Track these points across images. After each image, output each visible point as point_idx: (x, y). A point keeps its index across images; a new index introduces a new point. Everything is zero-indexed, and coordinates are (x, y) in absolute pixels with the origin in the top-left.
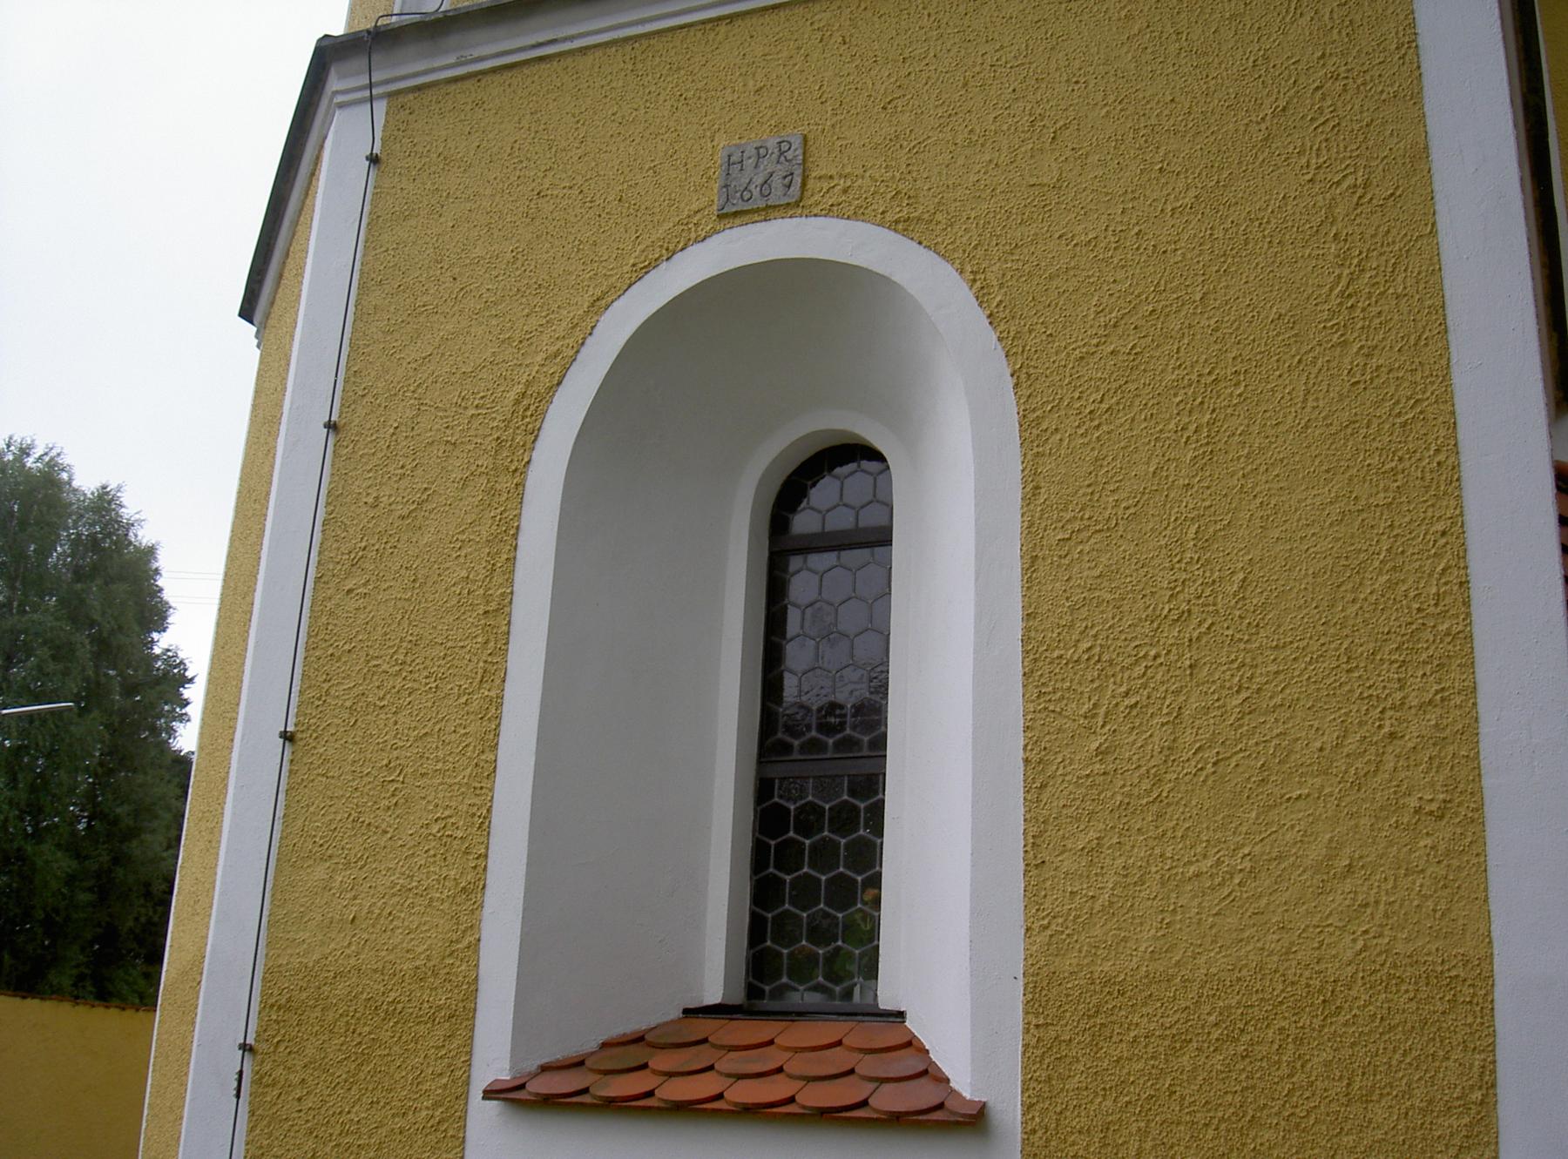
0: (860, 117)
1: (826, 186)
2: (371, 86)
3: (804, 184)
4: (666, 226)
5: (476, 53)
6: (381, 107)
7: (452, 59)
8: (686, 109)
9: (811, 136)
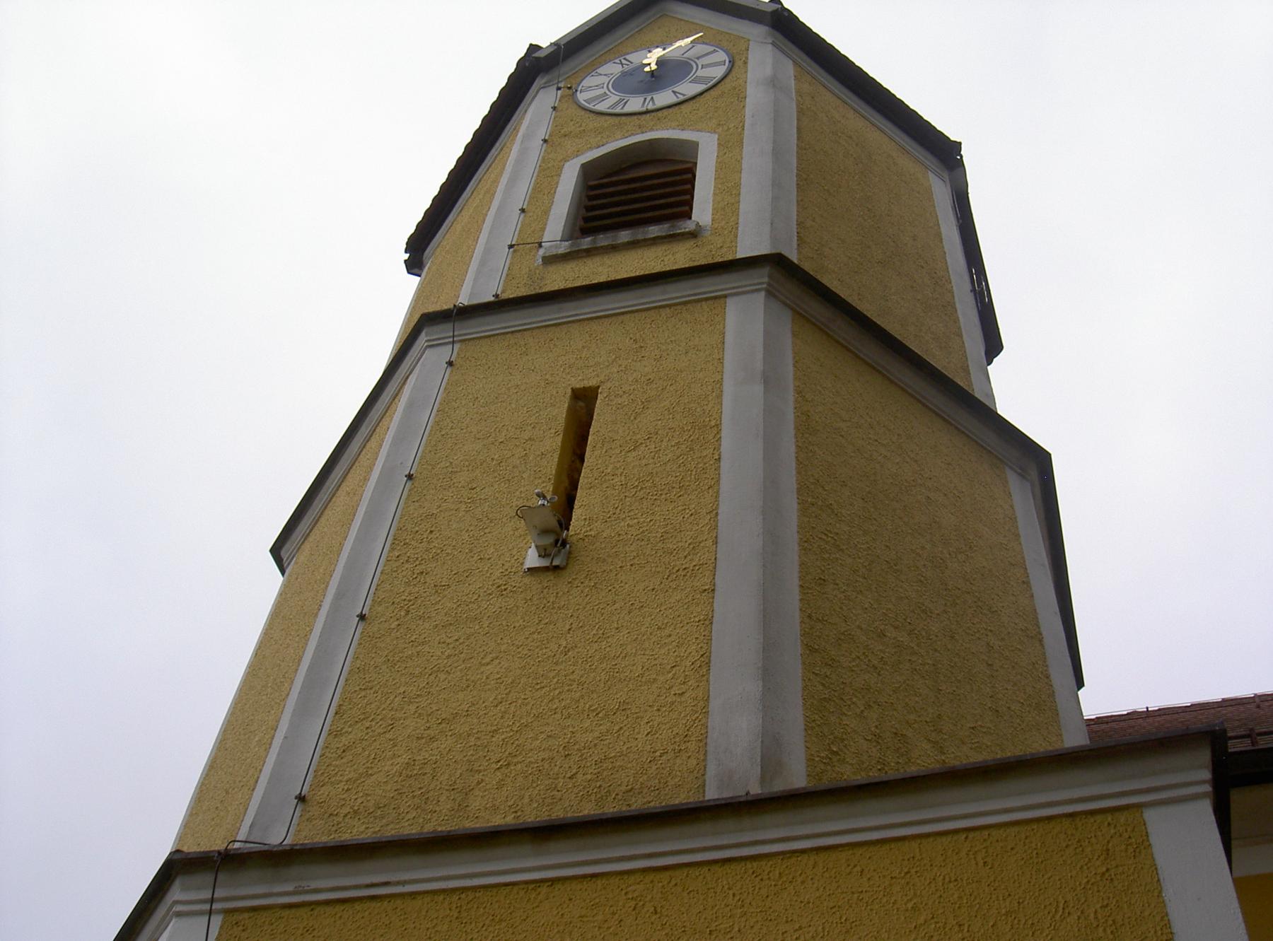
2: (212, 901)
5: (314, 884)
6: (217, 921)
7: (290, 888)
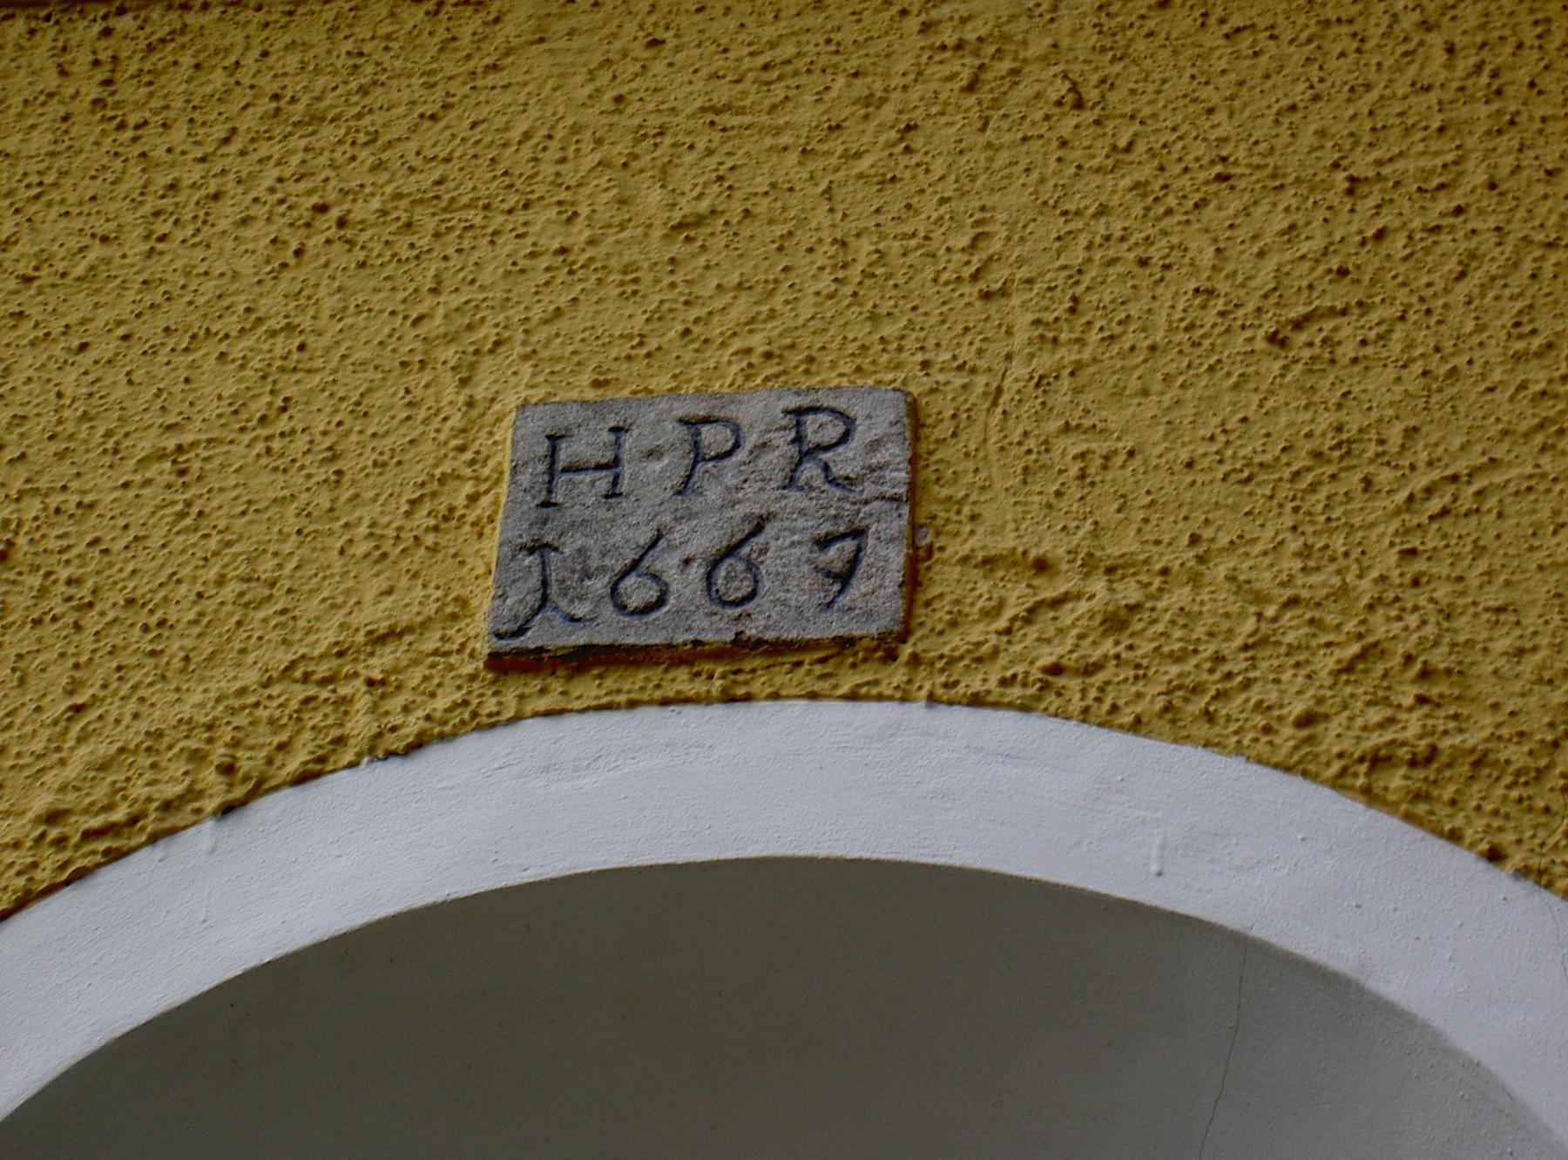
0: (1169, 363)
1: (1017, 597)
3: (913, 582)
4: (221, 681)
8: (341, 258)
9: (941, 406)
